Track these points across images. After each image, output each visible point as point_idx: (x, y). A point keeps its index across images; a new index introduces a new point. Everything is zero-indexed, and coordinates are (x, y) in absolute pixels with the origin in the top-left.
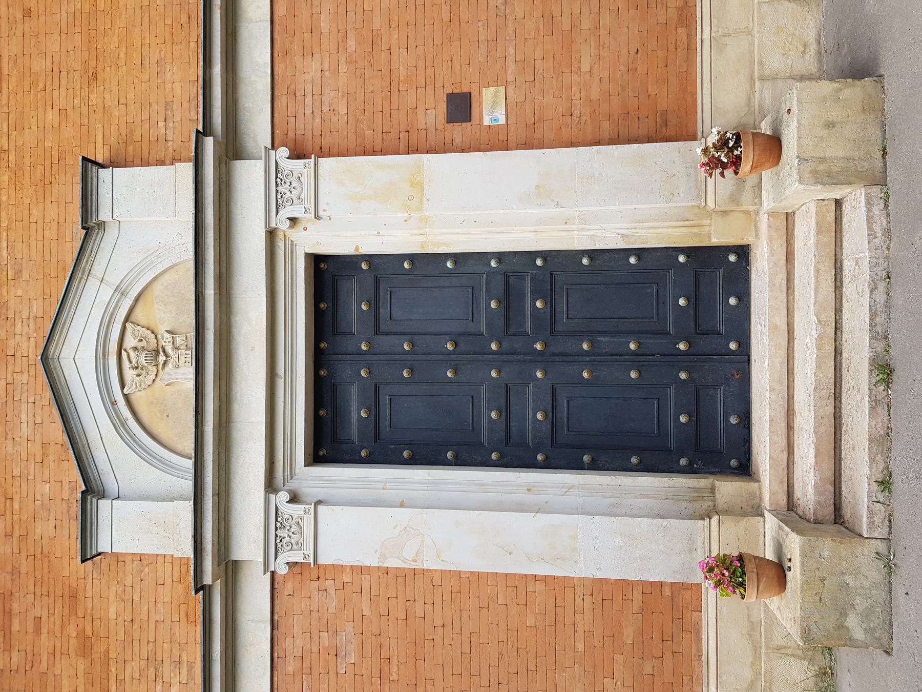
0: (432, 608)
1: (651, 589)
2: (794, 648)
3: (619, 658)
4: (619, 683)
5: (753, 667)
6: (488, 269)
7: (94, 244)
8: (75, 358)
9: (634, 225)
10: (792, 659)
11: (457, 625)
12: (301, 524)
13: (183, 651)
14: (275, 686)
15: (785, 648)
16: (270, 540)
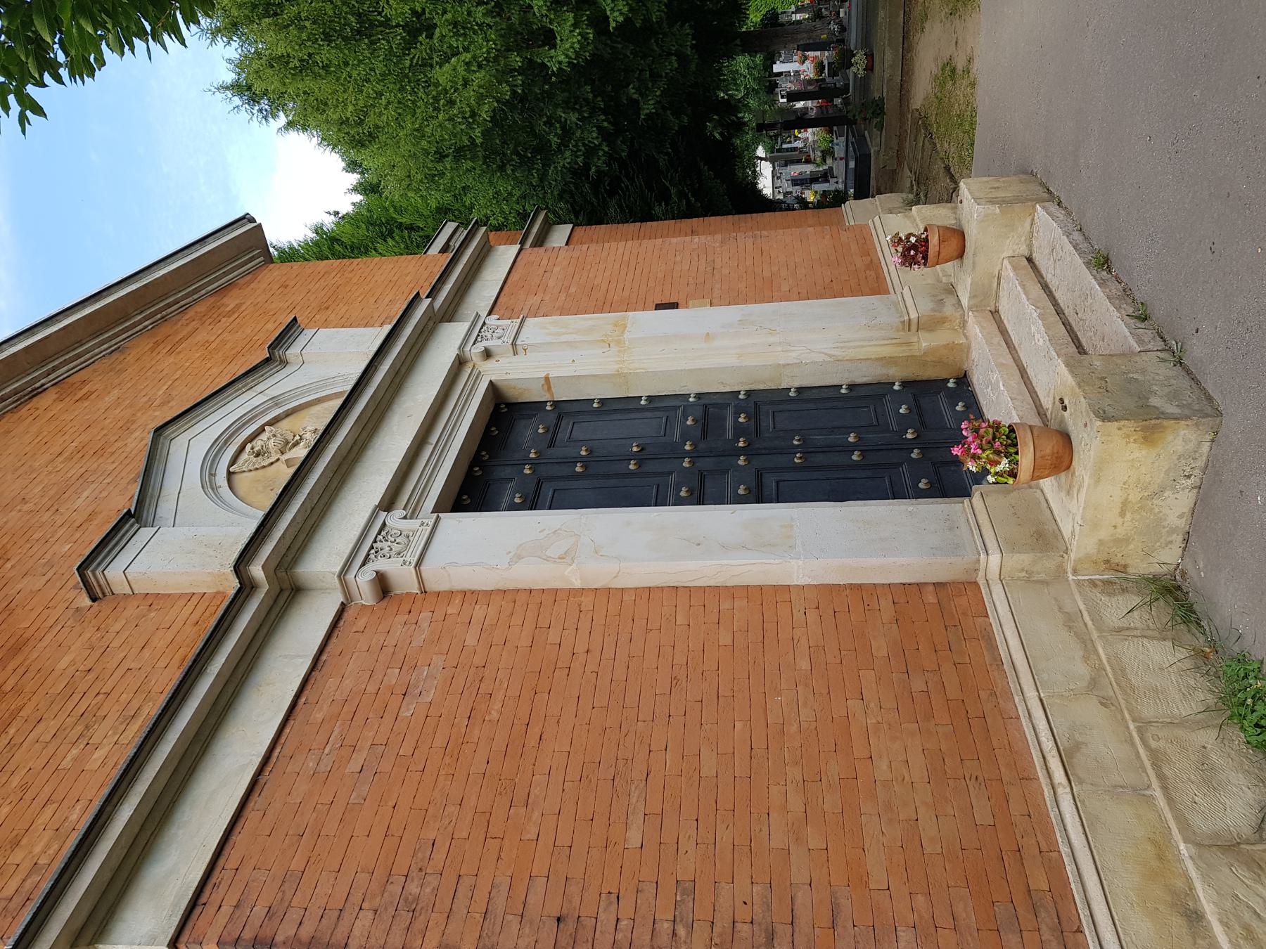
0: (574, 634)
1: (908, 592)
2: (1143, 629)
3: (868, 677)
4: (872, 705)
5: (1088, 662)
6: (686, 403)
7: (268, 371)
8: (191, 441)
9: (841, 345)
10: (1145, 641)
11: (608, 653)
12: (411, 539)
13: (149, 701)
14: (282, 740)
15: (1128, 629)
16: (353, 565)
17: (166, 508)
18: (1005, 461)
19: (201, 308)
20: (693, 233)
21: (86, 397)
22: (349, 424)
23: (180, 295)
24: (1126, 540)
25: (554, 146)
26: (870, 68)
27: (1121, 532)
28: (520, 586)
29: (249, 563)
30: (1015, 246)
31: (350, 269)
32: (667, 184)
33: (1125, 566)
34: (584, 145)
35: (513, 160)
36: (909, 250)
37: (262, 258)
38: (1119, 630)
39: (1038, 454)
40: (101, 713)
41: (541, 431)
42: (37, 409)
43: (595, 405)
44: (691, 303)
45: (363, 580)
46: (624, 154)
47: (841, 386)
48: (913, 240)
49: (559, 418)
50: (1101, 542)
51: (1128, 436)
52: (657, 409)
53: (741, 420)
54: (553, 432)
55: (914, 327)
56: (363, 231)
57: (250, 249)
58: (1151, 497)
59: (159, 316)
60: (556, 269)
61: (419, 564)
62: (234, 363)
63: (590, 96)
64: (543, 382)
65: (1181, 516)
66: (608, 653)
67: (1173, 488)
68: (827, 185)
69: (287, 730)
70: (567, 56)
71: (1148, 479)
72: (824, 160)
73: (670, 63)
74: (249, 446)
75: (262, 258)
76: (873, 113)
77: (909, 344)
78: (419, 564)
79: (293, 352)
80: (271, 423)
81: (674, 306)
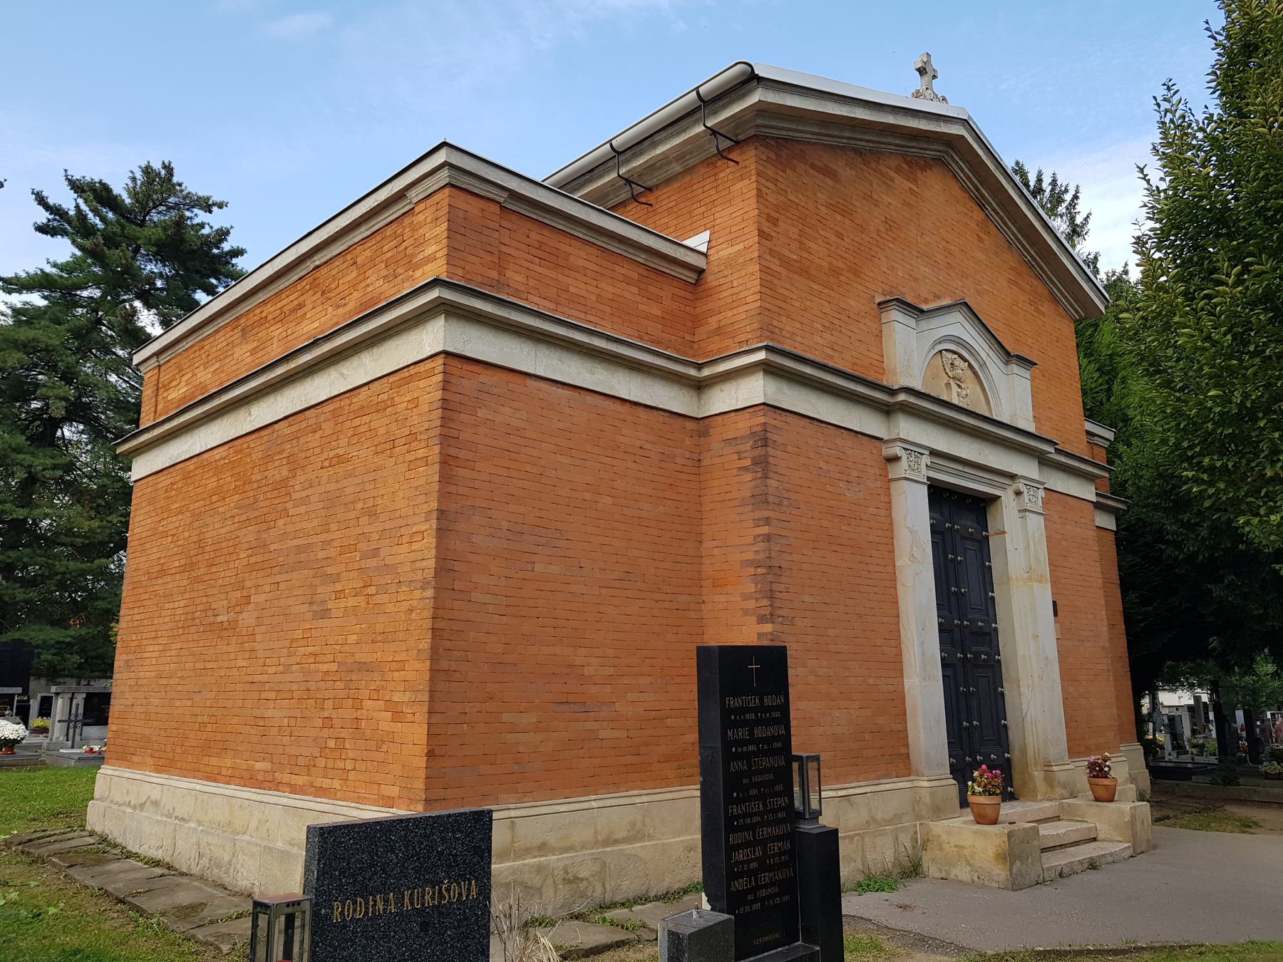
17: (924, 324)
18: (981, 790)
19: (1041, 288)
20: (1112, 626)
21: (980, 239)
22: (833, 109)
23: (1049, 273)
24: (941, 849)
25: (1181, 517)
26: (1267, 776)
27: (946, 846)
28: (895, 532)
29: (906, 392)
30: (1103, 830)
31: (1073, 383)
32: (1155, 604)
33: (926, 849)
34: (1183, 540)
35: (1168, 485)
36: (1099, 766)
37: (1077, 317)
38: (897, 838)
39: (986, 806)
40: (834, 333)
41: (970, 530)
42: (972, 212)
43: (987, 563)
44: (1058, 625)
45: (897, 450)
46: (1177, 570)
47: (1005, 720)
48: (1106, 769)
49: (979, 541)
50: (939, 836)
51: (1000, 846)
52: (987, 603)
53: (983, 656)
54: (970, 538)
55: (1047, 768)
56: (1105, 351)
57: (1084, 309)
58: (966, 860)
59: (1034, 263)
60: (1078, 530)
61: (906, 479)
62: (1004, 326)
63: (1223, 546)
64: (1002, 530)
65: (956, 876)
66: (869, 582)
67: (972, 871)
68: (1170, 748)
69: (832, 427)
70: (1249, 532)
71: (977, 858)
72: (1194, 746)
73: (1257, 609)
74: (956, 356)
75: (1077, 317)
76: (1225, 776)
77: (1036, 765)
78: (906, 479)
79: (1015, 368)
80: (970, 366)
81: (1056, 614)
